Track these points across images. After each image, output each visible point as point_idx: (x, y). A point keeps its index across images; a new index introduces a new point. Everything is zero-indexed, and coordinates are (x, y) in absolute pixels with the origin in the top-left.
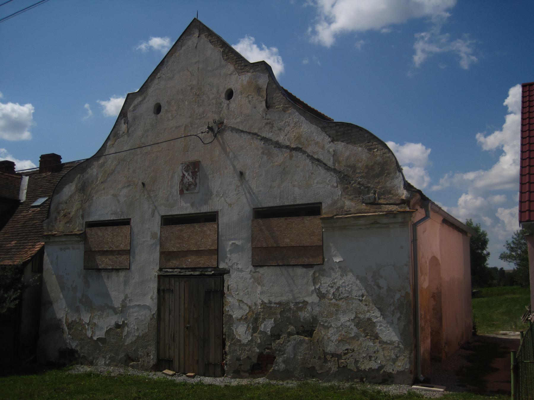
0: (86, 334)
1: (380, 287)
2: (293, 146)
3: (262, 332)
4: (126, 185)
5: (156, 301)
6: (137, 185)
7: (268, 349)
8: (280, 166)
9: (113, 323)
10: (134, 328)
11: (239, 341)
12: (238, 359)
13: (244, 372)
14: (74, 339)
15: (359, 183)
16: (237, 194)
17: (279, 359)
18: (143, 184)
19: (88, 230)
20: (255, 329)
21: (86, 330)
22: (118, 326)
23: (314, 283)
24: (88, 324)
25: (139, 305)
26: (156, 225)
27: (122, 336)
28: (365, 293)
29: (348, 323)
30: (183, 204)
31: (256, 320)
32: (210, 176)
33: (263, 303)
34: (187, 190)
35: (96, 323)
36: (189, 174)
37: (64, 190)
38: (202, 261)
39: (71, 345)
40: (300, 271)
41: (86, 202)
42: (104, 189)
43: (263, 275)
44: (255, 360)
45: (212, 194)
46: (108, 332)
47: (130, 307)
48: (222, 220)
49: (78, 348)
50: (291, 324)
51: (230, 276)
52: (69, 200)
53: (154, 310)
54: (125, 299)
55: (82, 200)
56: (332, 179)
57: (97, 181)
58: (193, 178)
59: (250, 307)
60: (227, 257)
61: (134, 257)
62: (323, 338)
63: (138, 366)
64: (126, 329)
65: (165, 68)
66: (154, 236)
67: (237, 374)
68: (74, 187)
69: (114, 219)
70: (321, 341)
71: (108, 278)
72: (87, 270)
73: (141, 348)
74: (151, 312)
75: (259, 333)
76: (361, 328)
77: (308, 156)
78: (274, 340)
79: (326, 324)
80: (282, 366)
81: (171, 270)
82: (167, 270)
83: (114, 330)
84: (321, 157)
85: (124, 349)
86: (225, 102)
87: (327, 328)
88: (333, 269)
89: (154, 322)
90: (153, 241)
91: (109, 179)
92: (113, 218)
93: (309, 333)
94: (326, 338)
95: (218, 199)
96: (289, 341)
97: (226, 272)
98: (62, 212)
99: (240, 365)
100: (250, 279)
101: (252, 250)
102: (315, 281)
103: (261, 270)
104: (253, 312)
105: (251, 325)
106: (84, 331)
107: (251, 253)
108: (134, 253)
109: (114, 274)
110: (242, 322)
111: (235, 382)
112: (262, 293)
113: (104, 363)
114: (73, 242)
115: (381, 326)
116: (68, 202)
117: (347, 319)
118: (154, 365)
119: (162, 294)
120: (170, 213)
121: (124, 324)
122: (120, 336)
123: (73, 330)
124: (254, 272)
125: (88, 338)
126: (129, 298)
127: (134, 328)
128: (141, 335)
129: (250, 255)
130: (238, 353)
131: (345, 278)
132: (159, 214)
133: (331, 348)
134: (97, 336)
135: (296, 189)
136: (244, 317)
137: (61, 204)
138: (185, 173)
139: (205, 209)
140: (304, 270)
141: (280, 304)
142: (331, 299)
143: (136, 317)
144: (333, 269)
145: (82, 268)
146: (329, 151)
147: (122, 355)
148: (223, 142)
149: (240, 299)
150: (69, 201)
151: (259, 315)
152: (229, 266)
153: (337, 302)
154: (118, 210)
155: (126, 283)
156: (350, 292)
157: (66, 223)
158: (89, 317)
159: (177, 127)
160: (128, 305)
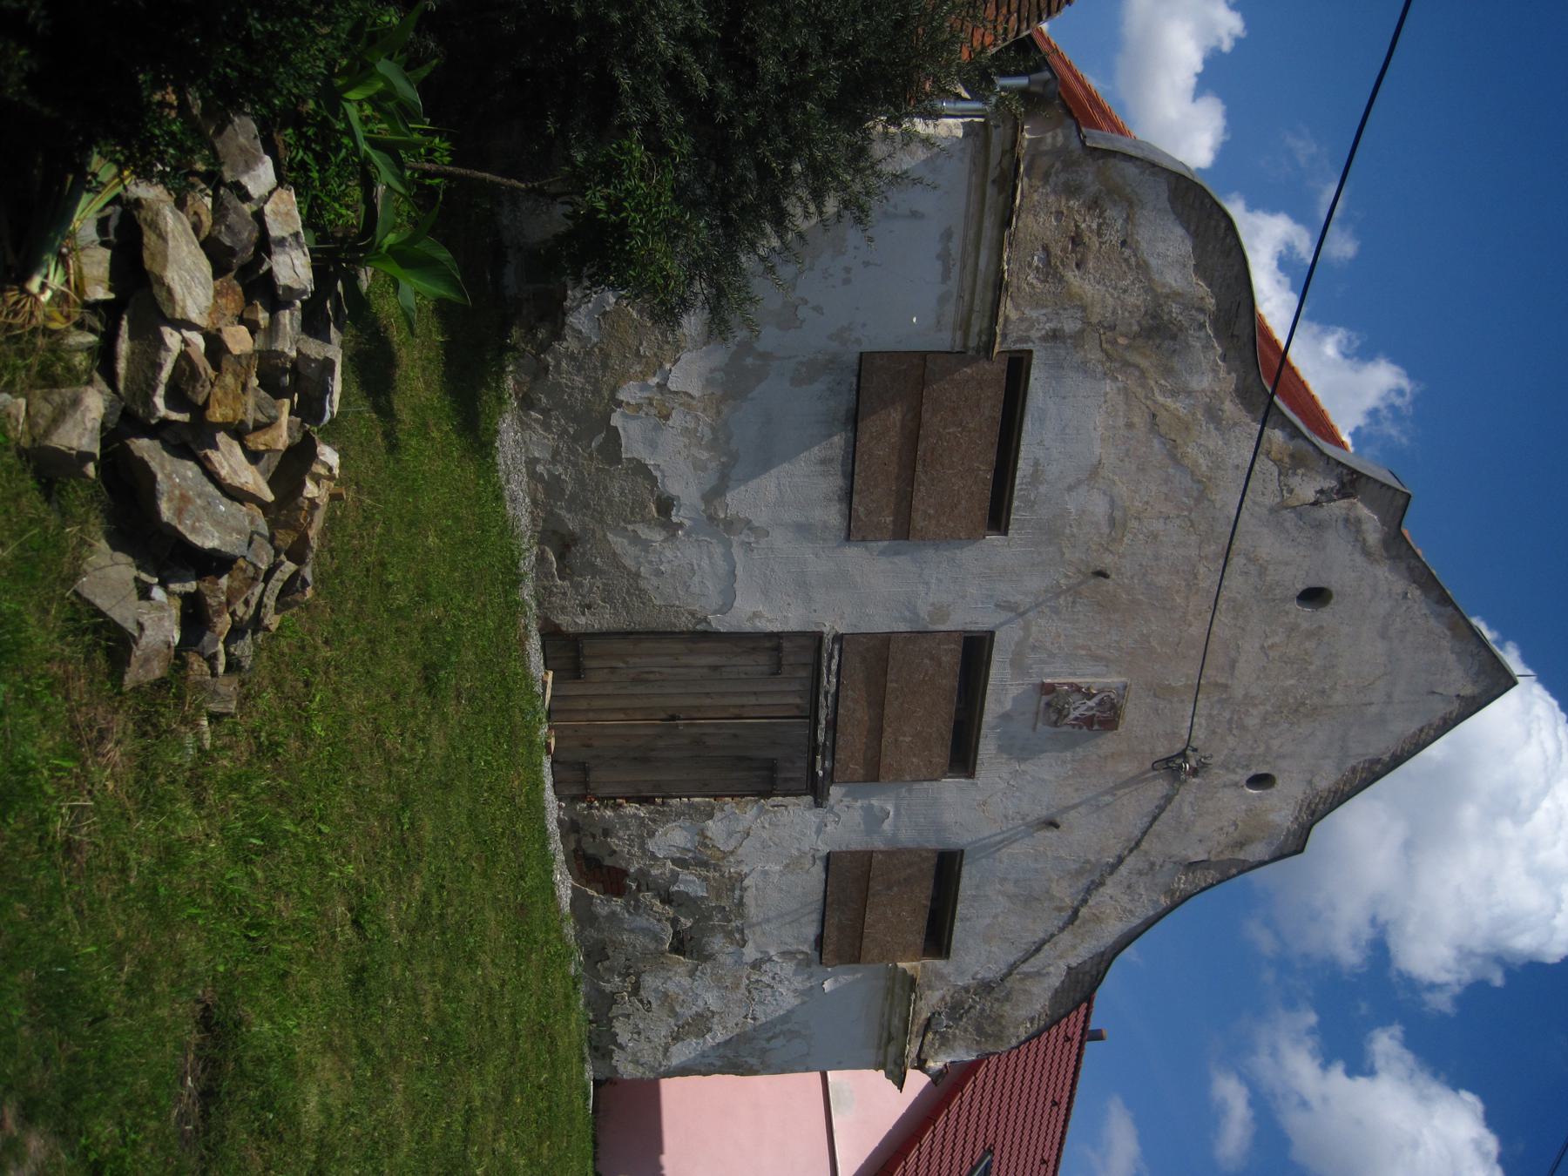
0: (625, 376)
1: (769, 1040)
2: (1083, 911)
3: (675, 876)
4: (1118, 514)
5: (747, 627)
6: (1107, 549)
7: (638, 886)
8: (1047, 892)
9: (673, 488)
10: (662, 563)
11: (652, 834)
12: (607, 833)
13: (578, 842)
14: (602, 323)
15: (971, 1007)
16: (1006, 817)
17: (617, 903)
18: (1102, 574)
19: (996, 369)
20: (681, 863)
21: (644, 375)
22: (666, 505)
23: (783, 954)
24: (662, 387)
25: (735, 576)
26: (967, 617)
27: (635, 522)
28: (758, 1023)
29: (700, 1003)
30: (1014, 691)
31: (705, 864)
32: (1069, 754)
33: (741, 877)
34: (1048, 705)
35: (670, 423)
36: (1091, 708)
37: (1179, 231)
38: (853, 740)
39: (579, 306)
40: (811, 931)
41: (1103, 350)
42: (1130, 426)
43: (807, 872)
44: (608, 862)
45: (1021, 760)
46: (640, 469)
47: (728, 545)
48: (950, 788)
49: (571, 344)
50: (696, 922)
51: (810, 808)
52: (1133, 261)
53: (719, 623)
54: (752, 529)
55: (1113, 328)
56: (992, 971)
57: (1163, 390)
58: (1076, 719)
59: (732, 853)
60: (856, 800)
61: (882, 553)
62: (670, 970)
63: (546, 577)
64: (657, 536)
65: (1423, 612)
66: (940, 612)
67: (571, 828)
68: (1174, 284)
69: (1019, 474)
70: (663, 969)
71: (823, 462)
72: (856, 367)
73: (604, 584)
74: (715, 613)
75: (672, 871)
76: (693, 1019)
77: (1052, 936)
78: (658, 895)
79: (698, 973)
80: (602, 910)
81: (834, 667)
82: (837, 657)
83: (652, 492)
84: (1041, 955)
85: (594, 531)
86: (1243, 776)
87: (692, 974)
88: (809, 978)
89: (684, 623)
90: (924, 611)
91: (1156, 443)
92: (1023, 467)
93: (679, 946)
94: (671, 974)
95: (1005, 776)
96: (659, 921)
97: (819, 798)
98: (1094, 226)
99: (594, 836)
100: (799, 850)
101: (865, 852)
102: (787, 955)
103: (818, 871)
104: (723, 858)
105: (690, 855)
106: (638, 368)
107: (859, 848)
108: (897, 553)
109: (836, 482)
110: (697, 838)
111: (552, 826)
112: (765, 873)
113: (537, 455)
114: (967, 297)
115: (698, 1044)
116: (1127, 252)
117: (710, 1001)
118: (557, 626)
119: (768, 644)
120: (996, 657)
121: (671, 528)
122: (632, 513)
123: (635, 315)
124: (813, 856)
125: (614, 391)
126: (757, 542)
127: (662, 563)
128: (643, 584)
129: (854, 847)
130: (621, 833)
131: (791, 994)
132: (1002, 624)
133: (650, 982)
134: (624, 429)
135: (988, 921)
136: (708, 842)
137: (1128, 219)
138: (1096, 700)
139: (987, 748)
140: (812, 938)
141: (741, 903)
142: (748, 978)
143: (696, 567)
144: (809, 978)
145: (867, 347)
146: (1049, 965)
147: (572, 523)
148: (1146, 779)
149: (752, 833)
150: (1126, 260)
151: (715, 870)
152: (832, 807)
153: (743, 986)
154: (1043, 489)
155: (804, 530)
156: (761, 1003)
157: (1046, 248)
158: (690, 391)
159: (1233, 665)
160: (735, 539)
